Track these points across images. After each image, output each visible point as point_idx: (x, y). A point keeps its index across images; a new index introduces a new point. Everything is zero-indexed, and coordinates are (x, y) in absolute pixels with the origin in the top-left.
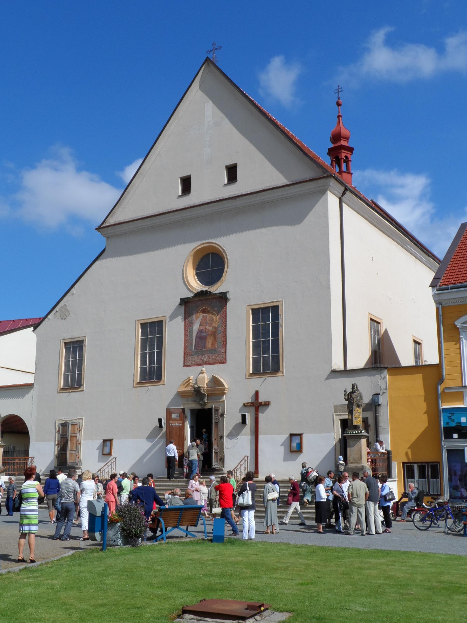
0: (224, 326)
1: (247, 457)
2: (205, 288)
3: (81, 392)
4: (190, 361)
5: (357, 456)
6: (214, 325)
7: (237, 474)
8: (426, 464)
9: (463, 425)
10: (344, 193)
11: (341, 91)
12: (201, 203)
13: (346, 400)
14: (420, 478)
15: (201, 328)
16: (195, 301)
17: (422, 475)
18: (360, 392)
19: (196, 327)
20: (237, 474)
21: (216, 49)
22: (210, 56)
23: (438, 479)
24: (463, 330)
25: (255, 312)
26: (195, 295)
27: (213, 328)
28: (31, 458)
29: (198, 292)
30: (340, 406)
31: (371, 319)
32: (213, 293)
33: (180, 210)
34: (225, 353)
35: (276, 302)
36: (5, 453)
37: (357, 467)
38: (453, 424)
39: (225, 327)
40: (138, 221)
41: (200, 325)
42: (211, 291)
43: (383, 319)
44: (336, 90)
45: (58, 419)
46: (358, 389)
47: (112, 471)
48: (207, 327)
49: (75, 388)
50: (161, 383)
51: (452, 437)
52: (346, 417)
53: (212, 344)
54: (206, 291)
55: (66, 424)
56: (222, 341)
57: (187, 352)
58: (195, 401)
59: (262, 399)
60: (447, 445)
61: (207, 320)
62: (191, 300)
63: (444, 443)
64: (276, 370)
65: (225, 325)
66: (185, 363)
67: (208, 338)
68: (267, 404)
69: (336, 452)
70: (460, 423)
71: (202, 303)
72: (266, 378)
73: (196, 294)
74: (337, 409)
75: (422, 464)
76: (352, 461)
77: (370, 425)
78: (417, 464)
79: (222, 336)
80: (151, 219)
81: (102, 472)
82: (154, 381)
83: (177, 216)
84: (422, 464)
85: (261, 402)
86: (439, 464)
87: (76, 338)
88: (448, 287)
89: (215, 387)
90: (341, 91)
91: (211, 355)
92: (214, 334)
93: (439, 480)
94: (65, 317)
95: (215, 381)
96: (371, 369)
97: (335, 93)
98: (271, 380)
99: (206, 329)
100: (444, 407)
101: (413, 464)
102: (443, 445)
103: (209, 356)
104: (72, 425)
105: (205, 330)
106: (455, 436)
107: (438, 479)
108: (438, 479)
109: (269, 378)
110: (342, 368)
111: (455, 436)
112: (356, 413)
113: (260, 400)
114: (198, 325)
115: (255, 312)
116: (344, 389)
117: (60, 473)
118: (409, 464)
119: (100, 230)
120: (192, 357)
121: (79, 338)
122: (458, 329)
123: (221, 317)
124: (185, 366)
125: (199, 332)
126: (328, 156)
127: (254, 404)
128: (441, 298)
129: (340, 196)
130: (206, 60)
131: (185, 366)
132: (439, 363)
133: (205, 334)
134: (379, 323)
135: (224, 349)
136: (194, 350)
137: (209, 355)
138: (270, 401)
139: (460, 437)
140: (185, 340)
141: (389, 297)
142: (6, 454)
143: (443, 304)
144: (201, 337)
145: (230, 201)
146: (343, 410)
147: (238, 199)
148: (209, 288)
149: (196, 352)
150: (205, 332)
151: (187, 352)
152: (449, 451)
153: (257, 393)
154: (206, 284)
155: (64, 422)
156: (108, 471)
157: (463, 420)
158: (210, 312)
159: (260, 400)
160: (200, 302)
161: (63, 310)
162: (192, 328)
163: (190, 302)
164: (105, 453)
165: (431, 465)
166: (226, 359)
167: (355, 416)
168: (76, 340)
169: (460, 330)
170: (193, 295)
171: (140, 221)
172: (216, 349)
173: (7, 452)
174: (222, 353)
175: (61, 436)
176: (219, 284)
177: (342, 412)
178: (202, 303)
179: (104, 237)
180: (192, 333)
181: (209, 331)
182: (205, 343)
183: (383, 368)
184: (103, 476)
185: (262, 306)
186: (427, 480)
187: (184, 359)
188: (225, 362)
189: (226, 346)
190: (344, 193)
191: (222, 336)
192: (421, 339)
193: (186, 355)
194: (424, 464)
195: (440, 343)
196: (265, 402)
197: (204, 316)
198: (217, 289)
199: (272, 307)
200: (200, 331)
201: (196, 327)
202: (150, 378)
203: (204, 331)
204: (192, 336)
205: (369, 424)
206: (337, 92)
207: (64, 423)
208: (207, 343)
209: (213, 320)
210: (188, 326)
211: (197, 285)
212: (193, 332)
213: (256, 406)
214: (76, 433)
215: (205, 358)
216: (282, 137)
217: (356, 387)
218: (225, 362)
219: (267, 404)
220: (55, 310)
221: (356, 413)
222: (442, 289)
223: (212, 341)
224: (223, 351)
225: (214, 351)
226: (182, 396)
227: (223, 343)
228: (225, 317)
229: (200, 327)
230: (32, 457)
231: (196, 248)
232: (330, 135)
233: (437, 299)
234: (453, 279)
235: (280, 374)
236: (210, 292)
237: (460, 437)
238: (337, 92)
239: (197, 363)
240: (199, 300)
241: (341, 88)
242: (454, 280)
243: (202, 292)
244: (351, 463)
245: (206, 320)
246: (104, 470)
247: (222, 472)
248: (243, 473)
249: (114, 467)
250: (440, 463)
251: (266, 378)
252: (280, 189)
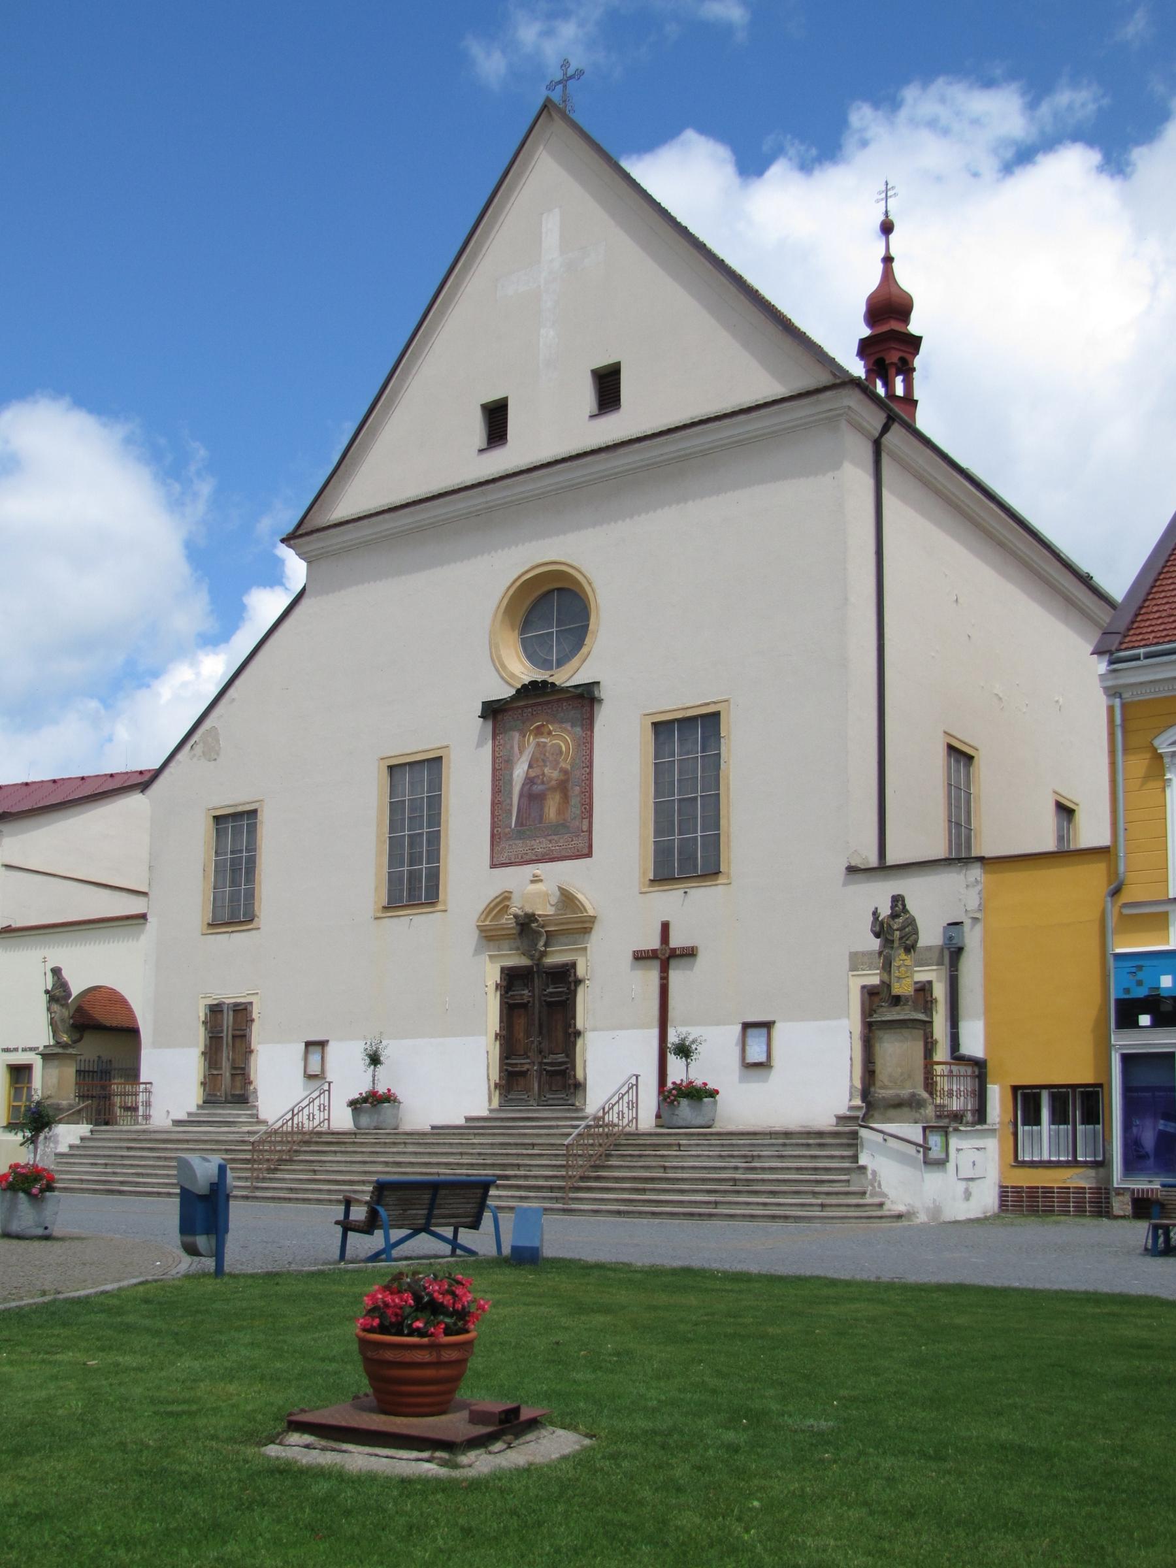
0: (588, 767)
1: (635, 1077)
2: (539, 675)
3: (254, 932)
4: (506, 854)
5: (899, 1070)
6: (563, 765)
7: (611, 1116)
8: (1069, 1090)
9: (1163, 994)
10: (885, 429)
11: (891, 197)
12: (532, 466)
13: (877, 935)
14: (1053, 1124)
15: (532, 774)
16: (518, 708)
17: (1060, 1117)
18: (911, 915)
19: (520, 771)
20: (611, 1116)
21: (571, 78)
22: (556, 96)
23: (1099, 1124)
24: (1172, 761)
25: (662, 729)
26: (516, 692)
27: (560, 772)
28: (144, 1086)
29: (524, 686)
30: (864, 954)
31: (951, 748)
32: (559, 686)
33: (481, 484)
34: (590, 831)
35: (714, 703)
36: (80, 1075)
37: (898, 1095)
38: (1140, 993)
39: (588, 770)
40: (381, 517)
41: (530, 766)
42: (556, 683)
43: (979, 747)
44: (880, 193)
45: (203, 996)
46: (908, 907)
47: (629, 1109)
48: (546, 770)
49: (241, 923)
50: (440, 907)
51: (1135, 1024)
52: (875, 980)
53: (560, 812)
54: (544, 682)
55: (222, 1007)
56: (583, 805)
57: (497, 831)
58: (518, 949)
59: (676, 941)
60: (1125, 1041)
61: (547, 754)
62: (507, 707)
63: (1115, 1038)
64: (712, 872)
65: (588, 764)
66: (495, 859)
67: (549, 796)
68: (690, 953)
69: (852, 1065)
70: (1158, 988)
71: (534, 713)
72: (686, 890)
73: (518, 691)
74: (856, 962)
75: (1034, 1091)
76: (886, 1083)
77: (936, 1000)
78: (1047, 1091)
79: (583, 792)
80: (412, 509)
81: (608, 1112)
82: (423, 904)
83: (476, 500)
84: (1034, 1091)
85: (675, 949)
86: (1102, 1092)
87: (240, 805)
88: (1139, 655)
89: (565, 915)
90: (891, 197)
91: (555, 838)
92: (563, 787)
93: (1100, 1127)
94: (215, 757)
95: (567, 899)
96: (942, 863)
97: (878, 201)
98: (702, 895)
99: (543, 774)
100: (1118, 951)
101: (1038, 1091)
102: (1113, 1042)
103: (550, 841)
104: (234, 1011)
105: (541, 777)
106: (1145, 1020)
107: (1097, 1126)
108: (1099, 1124)
109: (693, 890)
110: (873, 861)
111: (1145, 1020)
112: (899, 967)
113: (674, 943)
114: (526, 767)
115: (662, 729)
116: (873, 909)
117: (396, 1116)
118: (1029, 1091)
119: (292, 542)
120: (510, 845)
121: (247, 805)
122: (1160, 757)
123: (579, 745)
124: (493, 866)
125: (528, 784)
126: (857, 359)
127: (659, 952)
128: (1121, 681)
129: (877, 434)
130: (545, 107)
131: (493, 866)
132: (1112, 842)
133: (541, 787)
134: (970, 758)
135: (586, 822)
136: (515, 827)
137: (550, 838)
138: (696, 945)
139: (1157, 1023)
140: (493, 804)
141: (997, 695)
142: (84, 1076)
143: (1124, 696)
144: (533, 796)
145: (603, 455)
146: (872, 963)
147: (622, 451)
148: (552, 676)
149: (519, 831)
150: (543, 783)
151: (497, 831)
152: (1127, 1059)
153: (665, 927)
154: (545, 664)
155: (215, 1002)
156: (311, 1111)
157: (1166, 982)
158: (554, 733)
159: (674, 943)
160: (530, 710)
161: (210, 739)
162: (511, 775)
163: (505, 710)
164: (311, 1072)
165: (1082, 1092)
166: (590, 847)
167: (897, 974)
168: (240, 809)
169: (1167, 760)
170: (512, 692)
171: (387, 516)
172: (568, 824)
173: (89, 1072)
174: (583, 832)
175: (210, 1035)
176: (575, 662)
177: (870, 970)
178: (534, 713)
179: (303, 561)
180: (511, 784)
181: (551, 779)
182: (542, 809)
183: (972, 860)
184: (300, 1124)
185: (679, 715)
186: (1070, 1127)
187: (492, 850)
188: (589, 854)
189: (591, 816)
190: (885, 429)
191: (583, 792)
192: (1075, 800)
193: (495, 838)
194: (1065, 1090)
195: (1113, 764)
196: (683, 948)
197: (538, 744)
198: (568, 676)
199: (703, 717)
200: (529, 781)
201: (520, 771)
202: (411, 896)
203: (539, 781)
204: (510, 792)
205: (934, 997)
206: (882, 199)
207: (216, 1005)
208: (546, 809)
209: (561, 752)
210: (501, 769)
211: (523, 670)
212: (514, 783)
213: (663, 957)
214: (245, 1028)
215: (541, 845)
216: (733, 289)
217: (900, 902)
218: (589, 854)
219: (690, 953)
220: (192, 742)
221: (899, 967)
222: (1129, 658)
223: (559, 803)
224: (585, 829)
225: (561, 828)
226: (486, 937)
227: (585, 808)
228: (588, 746)
229: (530, 770)
230: (146, 1083)
231: (519, 577)
232: (862, 308)
233: (1109, 683)
234: (1153, 635)
235: (722, 880)
236: (553, 684)
237: (1157, 1023)
238: (882, 199)
239: (522, 858)
240: (526, 707)
241: (893, 188)
242: (1155, 637)
243: (534, 683)
244: (884, 1087)
245: (545, 755)
246: (612, 1108)
247: (580, 1115)
248: (617, 1115)
249: (326, 1104)
250: (1105, 1087)
251: (686, 890)
252: (727, 421)
